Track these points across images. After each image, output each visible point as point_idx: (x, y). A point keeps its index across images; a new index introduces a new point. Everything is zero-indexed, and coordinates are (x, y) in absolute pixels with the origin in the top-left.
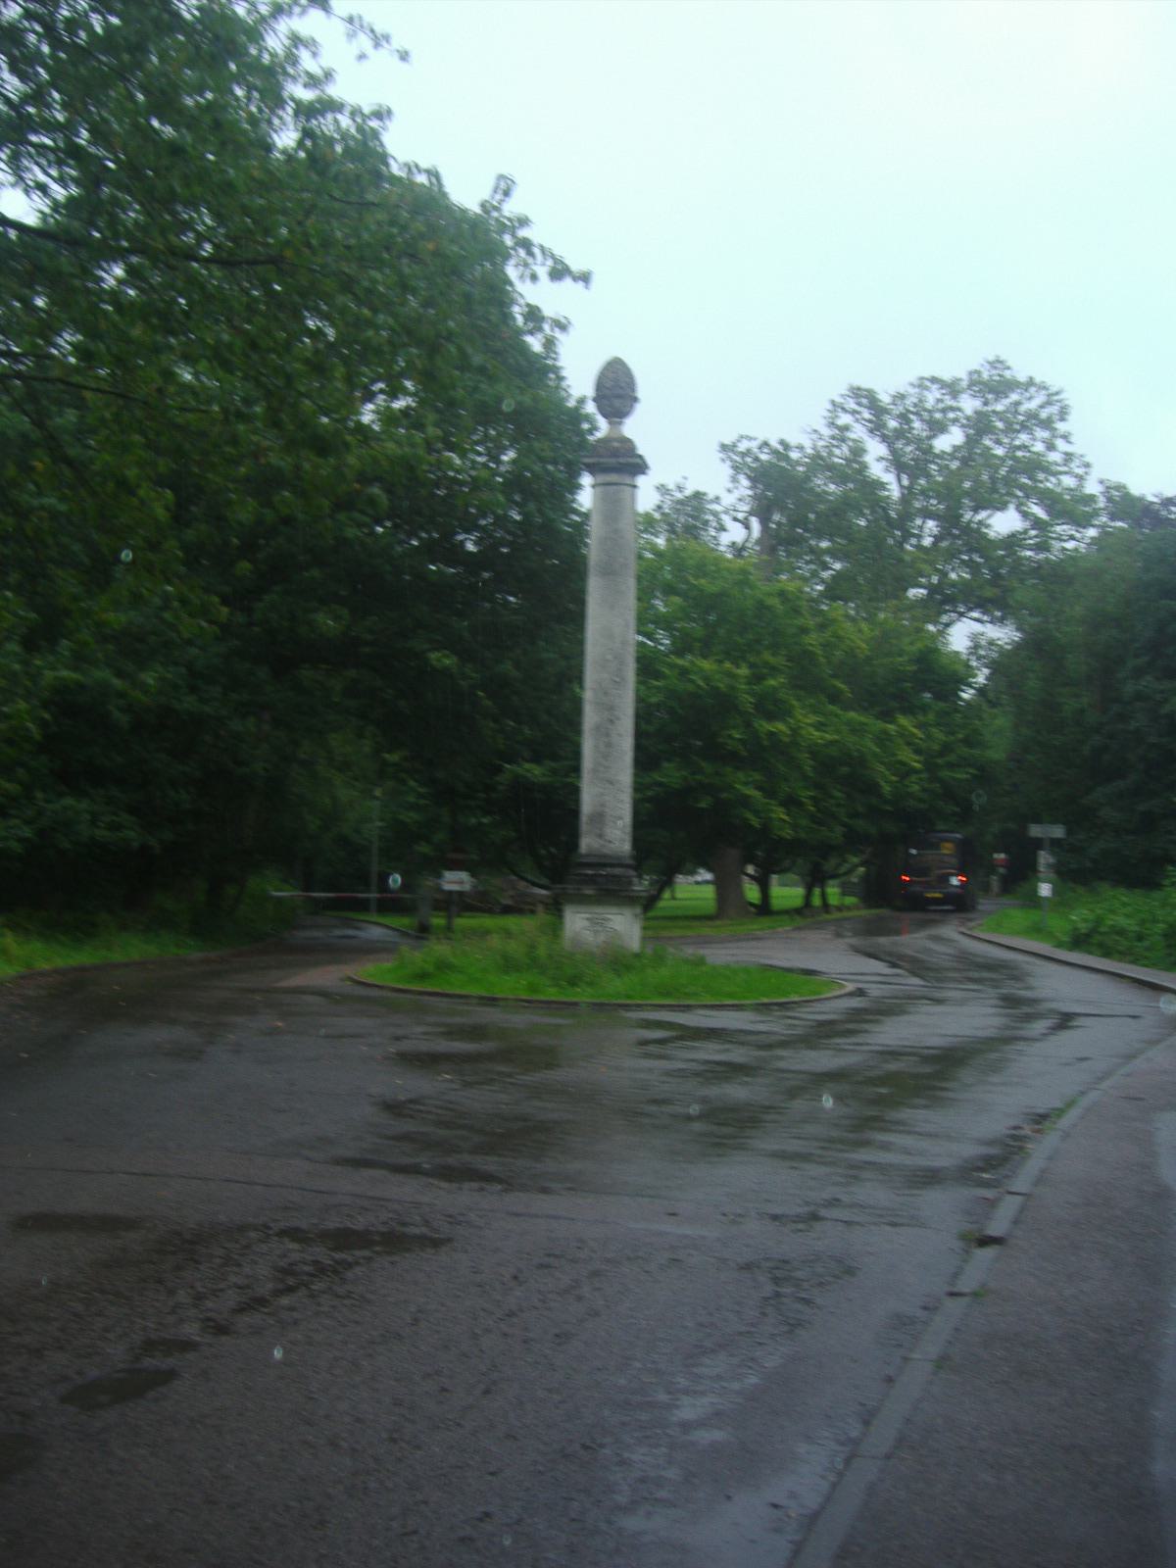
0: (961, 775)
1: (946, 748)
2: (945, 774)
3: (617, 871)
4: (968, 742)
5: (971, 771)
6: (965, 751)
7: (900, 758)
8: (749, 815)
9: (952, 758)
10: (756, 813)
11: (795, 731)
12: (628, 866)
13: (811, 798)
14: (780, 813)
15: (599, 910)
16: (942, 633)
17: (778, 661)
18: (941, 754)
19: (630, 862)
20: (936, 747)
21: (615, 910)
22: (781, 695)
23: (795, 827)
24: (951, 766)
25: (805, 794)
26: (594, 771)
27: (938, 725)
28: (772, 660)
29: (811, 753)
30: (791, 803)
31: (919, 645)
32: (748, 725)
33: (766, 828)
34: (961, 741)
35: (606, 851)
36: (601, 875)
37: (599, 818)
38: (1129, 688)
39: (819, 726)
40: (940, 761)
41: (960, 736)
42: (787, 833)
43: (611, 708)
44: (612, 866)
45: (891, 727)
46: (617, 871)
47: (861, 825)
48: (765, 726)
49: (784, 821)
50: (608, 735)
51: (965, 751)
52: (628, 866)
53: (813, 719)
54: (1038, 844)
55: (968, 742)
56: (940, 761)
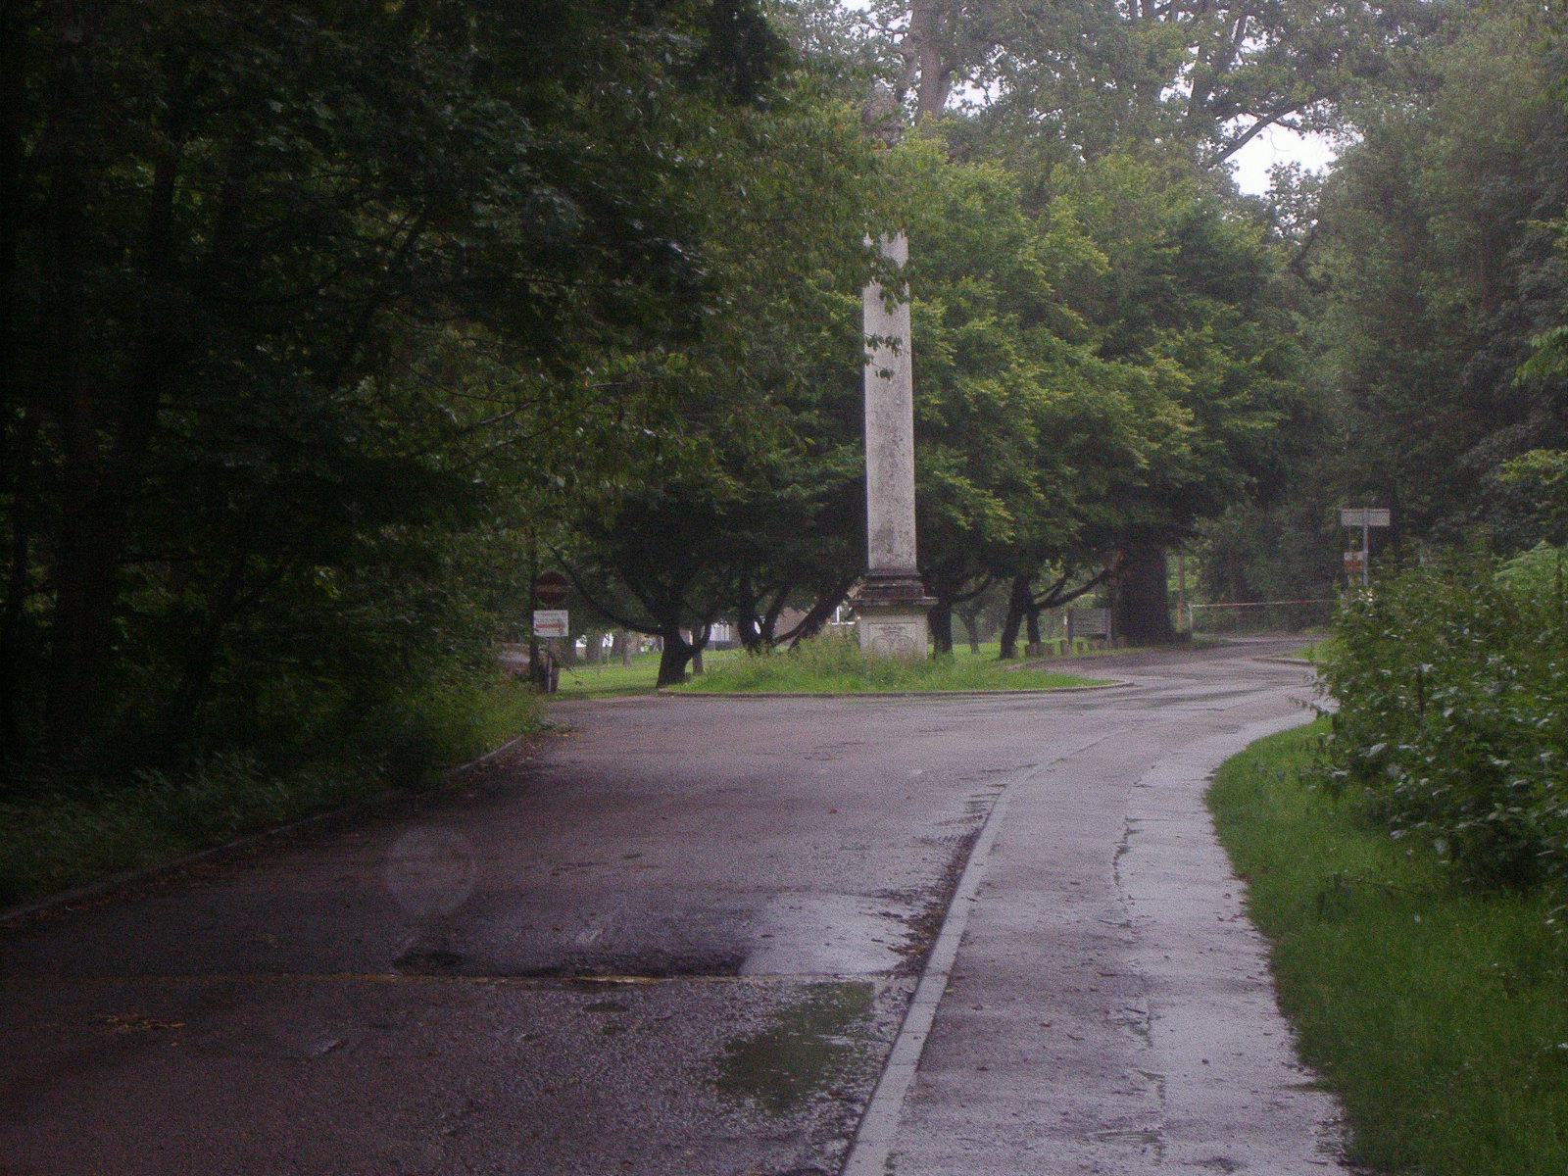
0: (1259, 424)
1: (1233, 383)
2: (1234, 423)
3: (908, 582)
4: (1270, 368)
5: (1277, 415)
6: (1266, 383)
7: (1159, 418)
8: (955, 513)
9: (1243, 396)
10: (965, 510)
11: (1014, 392)
12: (914, 578)
13: (1036, 479)
14: (996, 508)
15: (893, 619)
16: (1218, 159)
17: (983, 288)
18: (1226, 391)
19: (916, 573)
20: (1218, 381)
21: (907, 619)
22: (988, 338)
23: (1015, 525)
24: (1245, 409)
25: (1028, 476)
26: (881, 490)
27: (1217, 340)
28: (973, 287)
29: (1035, 417)
30: (1008, 488)
31: (1184, 207)
32: (947, 384)
33: (977, 532)
34: (1259, 367)
35: (895, 564)
36: (893, 588)
37: (887, 534)
38: (1526, 279)
39: (1042, 380)
40: (1224, 403)
41: (1257, 359)
42: (1007, 535)
43: (894, 430)
44: (904, 578)
45: (1145, 372)
46: (908, 582)
47: (1098, 512)
48: (972, 387)
49: (1002, 518)
50: (892, 455)
51: (1266, 383)
52: (914, 578)
53: (1035, 370)
54: (1346, 538)
55: (1270, 368)
56: (1224, 403)
